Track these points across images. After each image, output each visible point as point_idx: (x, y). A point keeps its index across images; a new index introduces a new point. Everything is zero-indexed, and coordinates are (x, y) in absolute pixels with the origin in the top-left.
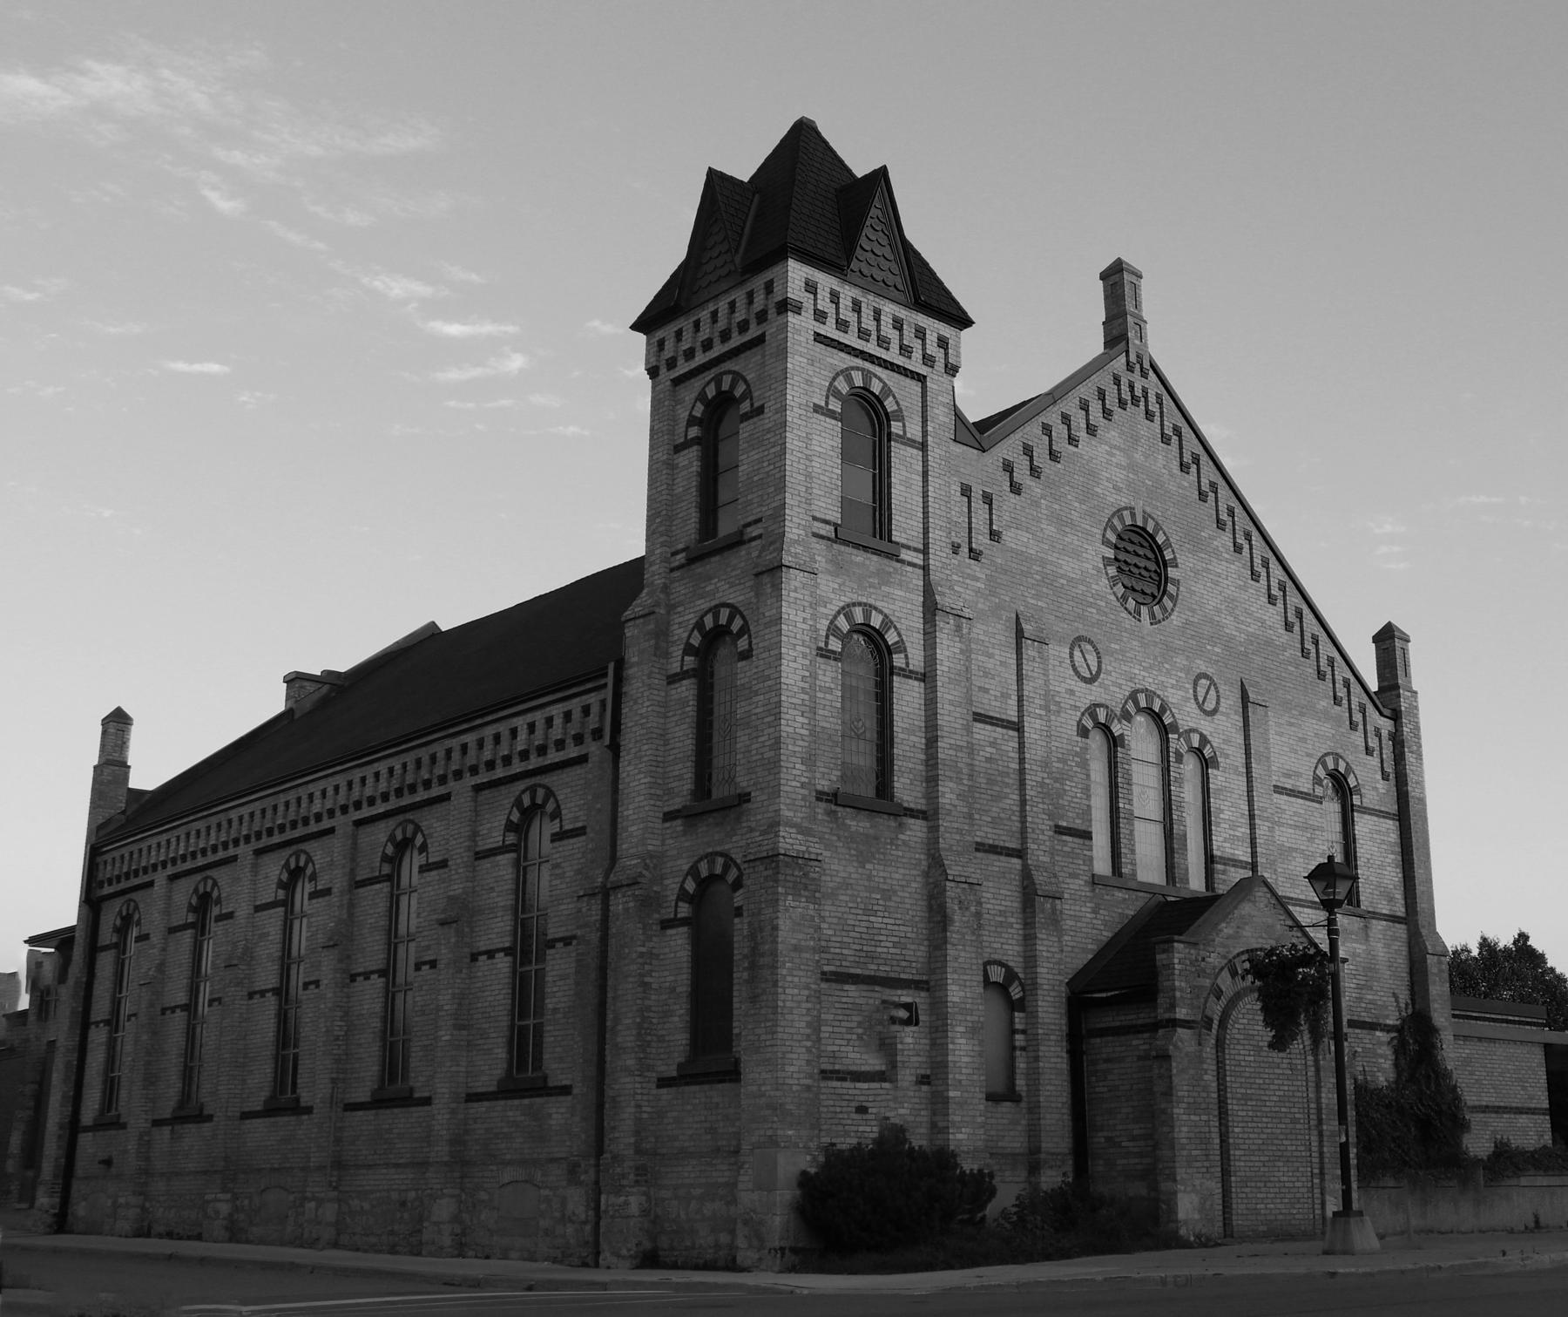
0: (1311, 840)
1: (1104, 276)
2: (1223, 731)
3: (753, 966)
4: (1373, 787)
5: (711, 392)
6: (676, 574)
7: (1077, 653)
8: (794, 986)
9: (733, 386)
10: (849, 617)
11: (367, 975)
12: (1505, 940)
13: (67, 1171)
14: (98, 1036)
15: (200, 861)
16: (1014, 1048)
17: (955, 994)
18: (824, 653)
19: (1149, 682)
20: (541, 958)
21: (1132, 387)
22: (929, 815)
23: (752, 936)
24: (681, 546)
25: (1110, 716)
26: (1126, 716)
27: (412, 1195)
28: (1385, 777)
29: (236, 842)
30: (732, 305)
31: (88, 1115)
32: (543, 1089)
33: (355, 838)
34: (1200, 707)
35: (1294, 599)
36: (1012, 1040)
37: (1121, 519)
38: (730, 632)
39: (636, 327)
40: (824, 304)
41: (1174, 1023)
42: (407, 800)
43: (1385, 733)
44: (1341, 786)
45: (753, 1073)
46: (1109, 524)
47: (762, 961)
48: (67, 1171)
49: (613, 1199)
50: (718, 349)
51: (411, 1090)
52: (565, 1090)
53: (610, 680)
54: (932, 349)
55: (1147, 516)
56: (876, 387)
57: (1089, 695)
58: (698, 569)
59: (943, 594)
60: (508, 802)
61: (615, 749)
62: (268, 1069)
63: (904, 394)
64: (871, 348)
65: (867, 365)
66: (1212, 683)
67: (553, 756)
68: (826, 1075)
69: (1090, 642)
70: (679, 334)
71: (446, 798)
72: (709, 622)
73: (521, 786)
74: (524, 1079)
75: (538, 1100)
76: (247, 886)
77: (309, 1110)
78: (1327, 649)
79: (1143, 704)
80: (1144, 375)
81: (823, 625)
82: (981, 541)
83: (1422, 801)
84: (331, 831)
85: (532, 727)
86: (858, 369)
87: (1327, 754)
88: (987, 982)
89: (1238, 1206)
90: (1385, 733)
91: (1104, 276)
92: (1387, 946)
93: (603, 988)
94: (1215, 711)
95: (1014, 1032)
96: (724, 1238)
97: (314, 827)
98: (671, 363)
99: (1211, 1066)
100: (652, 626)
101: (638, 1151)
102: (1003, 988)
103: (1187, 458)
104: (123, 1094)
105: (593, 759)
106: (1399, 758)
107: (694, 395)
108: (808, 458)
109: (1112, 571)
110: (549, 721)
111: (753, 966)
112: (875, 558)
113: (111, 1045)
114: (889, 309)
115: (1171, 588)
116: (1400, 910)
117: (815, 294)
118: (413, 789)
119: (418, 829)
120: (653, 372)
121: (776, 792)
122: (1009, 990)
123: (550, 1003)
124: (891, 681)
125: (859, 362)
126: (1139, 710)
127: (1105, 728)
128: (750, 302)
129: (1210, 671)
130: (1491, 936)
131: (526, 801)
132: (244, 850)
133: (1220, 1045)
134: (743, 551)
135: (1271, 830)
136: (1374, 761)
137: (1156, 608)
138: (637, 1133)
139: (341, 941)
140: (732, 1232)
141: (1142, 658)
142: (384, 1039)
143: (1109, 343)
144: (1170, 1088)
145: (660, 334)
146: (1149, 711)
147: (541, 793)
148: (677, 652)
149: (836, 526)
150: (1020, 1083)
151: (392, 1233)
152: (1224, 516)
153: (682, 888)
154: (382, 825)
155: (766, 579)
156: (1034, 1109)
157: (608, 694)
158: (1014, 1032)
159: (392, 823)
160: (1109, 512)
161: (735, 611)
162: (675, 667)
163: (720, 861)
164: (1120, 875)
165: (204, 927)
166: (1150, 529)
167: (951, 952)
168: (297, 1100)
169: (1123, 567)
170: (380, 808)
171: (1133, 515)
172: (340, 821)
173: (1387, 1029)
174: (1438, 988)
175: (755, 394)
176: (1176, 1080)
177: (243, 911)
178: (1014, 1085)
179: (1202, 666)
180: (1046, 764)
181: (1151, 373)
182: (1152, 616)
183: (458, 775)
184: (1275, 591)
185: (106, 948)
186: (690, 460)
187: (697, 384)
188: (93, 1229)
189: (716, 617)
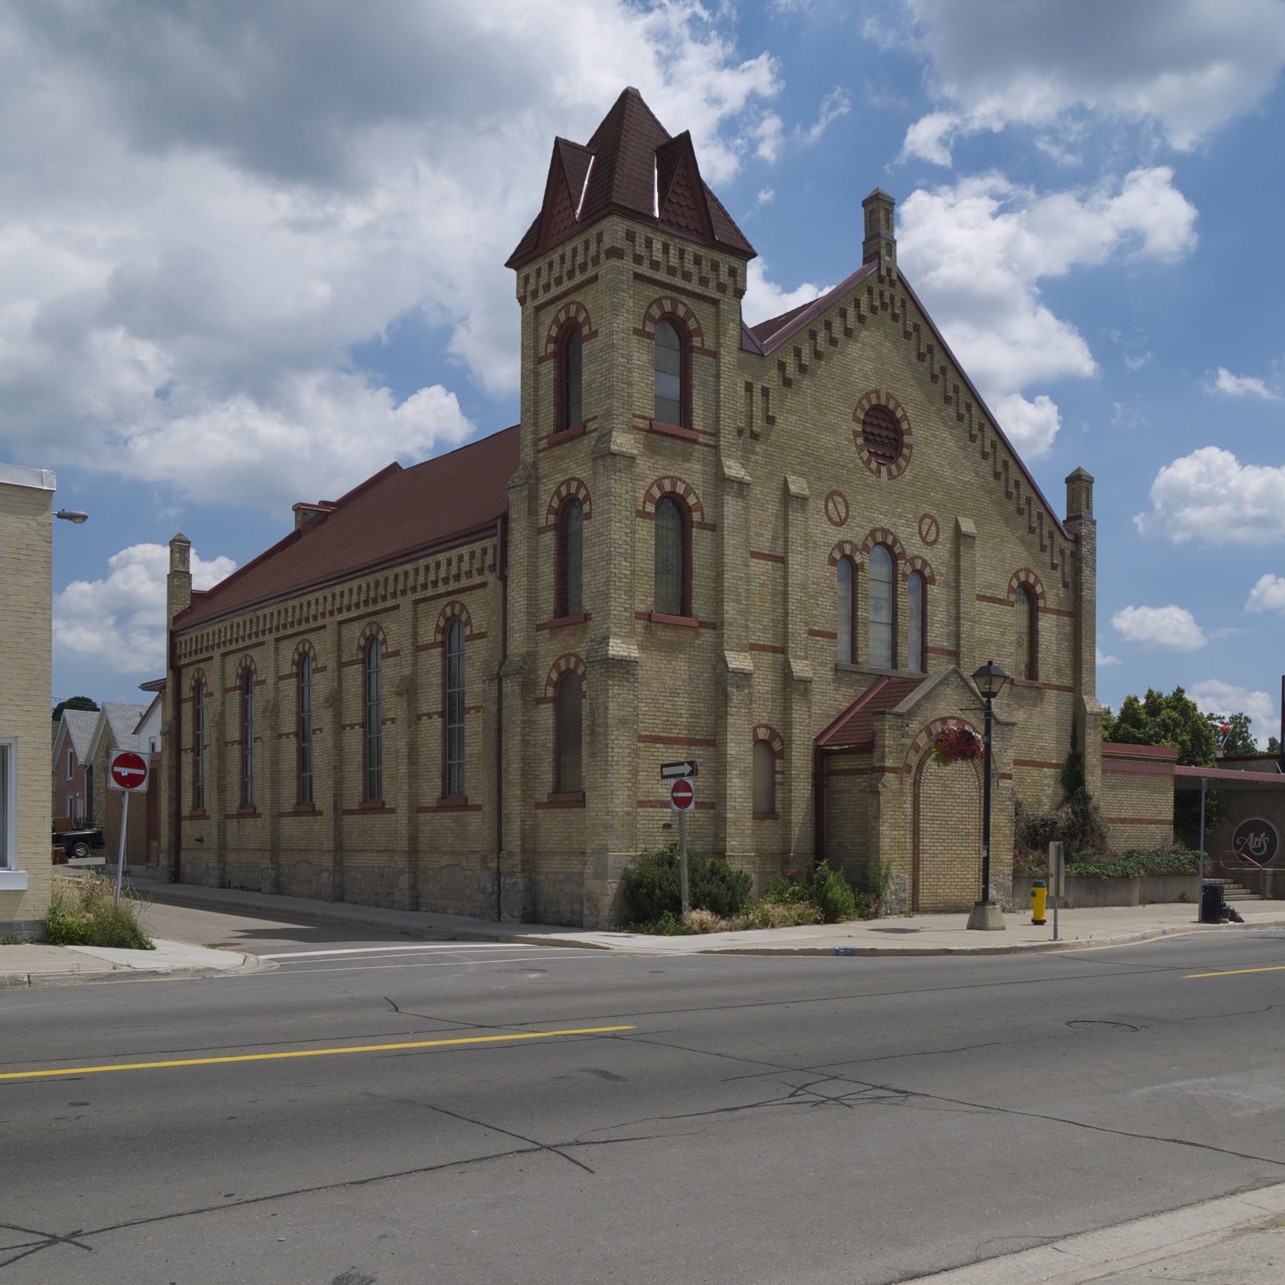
0: (1003, 634)
1: (865, 203)
2: (938, 557)
3: (593, 733)
4: (1052, 594)
5: (562, 317)
6: (541, 455)
7: (831, 504)
8: (619, 745)
9: (577, 313)
10: (660, 487)
11: (352, 726)
12: (1168, 692)
13: (177, 845)
14: (187, 759)
15: (241, 645)
16: (775, 784)
17: (732, 749)
18: (643, 514)
19: (885, 523)
20: (462, 720)
21: (881, 295)
22: (716, 625)
23: (592, 712)
24: (544, 434)
25: (855, 548)
26: (866, 548)
27: (387, 870)
28: (1065, 585)
29: (264, 633)
30: (575, 251)
31: (186, 808)
32: (465, 806)
33: (339, 632)
34: (923, 539)
35: (1002, 454)
36: (774, 778)
37: (869, 400)
39: (508, 265)
40: (641, 249)
41: (883, 770)
42: (372, 608)
43: (1067, 552)
44: (1028, 593)
45: (593, 803)
46: (860, 405)
47: (600, 730)
48: (177, 845)
49: (508, 880)
50: (567, 285)
51: (384, 803)
52: (478, 808)
53: (499, 529)
54: (724, 278)
55: (889, 396)
56: (681, 311)
57: (836, 535)
58: (557, 451)
59: (729, 467)
60: (437, 613)
61: (503, 578)
62: (294, 785)
63: (703, 313)
64: (678, 281)
65: (675, 295)
66: (934, 521)
67: (465, 582)
68: (642, 804)
69: (840, 495)
70: (539, 272)
71: (397, 607)
73: (445, 601)
74: (452, 799)
75: (464, 813)
76: (273, 663)
77: (321, 813)
78: (1025, 491)
79: (879, 539)
80: (892, 284)
81: (641, 494)
82: (759, 424)
83: (1093, 603)
84: (324, 627)
85: (449, 562)
86: (667, 298)
87: (1020, 570)
88: (757, 741)
89: (924, 885)
90: (1067, 552)
91: (865, 203)
92: (1057, 708)
93: (499, 742)
94: (935, 542)
95: (775, 772)
96: (577, 907)
97: (312, 624)
98: (535, 294)
99: (909, 799)
100: (526, 493)
101: (523, 850)
102: (766, 743)
103: (923, 349)
104: (206, 797)
105: (491, 585)
106: (1077, 571)
107: (550, 320)
108: (630, 371)
109: (860, 441)
110: (461, 558)
111: (593, 733)
112: (680, 442)
113: (196, 765)
114: (691, 249)
115: (906, 451)
116: (1067, 681)
117: (633, 241)
118: (375, 600)
119: (380, 628)
120: (522, 300)
121: (607, 615)
122: (772, 747)
123: (468, 750)
124: (691, 532)
125: (669, 293)
126: (877, 544)
127: (849, 558)
128: (587, 249)
129: (933, 512)
130: (1156, 690)
131: (449, 613)
132: (269, 638)
133: (917, 784)
134: (585, 440)
135: (972, 628)
136: (1058, 574)
137: (893, 467)
138: (522, 839)
139: (335, 701)
140: (582, 903)
141: (883, 506)
142: (365, 768)
143: (866, 260)
144: (878, 812)
145: (526, 271)
146: (884, 544)
147: (457, 607)
148: (543, 511)
149: (651, 420)
150: (778, 806)
151: (376, 893)
152: (950, 393)
153: (549, 677)
154: (356, 624)
155: (600, 462)
156: (787, 823)
157: (496, 540)
158: (775, 772)
159: (363, 623)
160: (859, 395)
161: (581, 484)
162: (542, 523)
163: (573, 659)
164: (857, 663)
165: (247, 689)
166: (891, 406)
167: (730, 720)
168: (314, 806)
169: (869, 437)
170: (354, 613)
171: (878, 397)
172: (328, 620)
173: (1051, 766)
174: (1093, 740)
175: (593, 321)
176: (882, 809)
177: (271, 681)
178: (774, 804)
179: (927, 509)
180: (804, 586)
181: (898, 283)
182: (890, 473)
183: (404, 592)
184: (988, 449)
185: (187, 700)
186: (548, 369)
187: (553, 309)
188: (196, 882)
189: (569, 487)
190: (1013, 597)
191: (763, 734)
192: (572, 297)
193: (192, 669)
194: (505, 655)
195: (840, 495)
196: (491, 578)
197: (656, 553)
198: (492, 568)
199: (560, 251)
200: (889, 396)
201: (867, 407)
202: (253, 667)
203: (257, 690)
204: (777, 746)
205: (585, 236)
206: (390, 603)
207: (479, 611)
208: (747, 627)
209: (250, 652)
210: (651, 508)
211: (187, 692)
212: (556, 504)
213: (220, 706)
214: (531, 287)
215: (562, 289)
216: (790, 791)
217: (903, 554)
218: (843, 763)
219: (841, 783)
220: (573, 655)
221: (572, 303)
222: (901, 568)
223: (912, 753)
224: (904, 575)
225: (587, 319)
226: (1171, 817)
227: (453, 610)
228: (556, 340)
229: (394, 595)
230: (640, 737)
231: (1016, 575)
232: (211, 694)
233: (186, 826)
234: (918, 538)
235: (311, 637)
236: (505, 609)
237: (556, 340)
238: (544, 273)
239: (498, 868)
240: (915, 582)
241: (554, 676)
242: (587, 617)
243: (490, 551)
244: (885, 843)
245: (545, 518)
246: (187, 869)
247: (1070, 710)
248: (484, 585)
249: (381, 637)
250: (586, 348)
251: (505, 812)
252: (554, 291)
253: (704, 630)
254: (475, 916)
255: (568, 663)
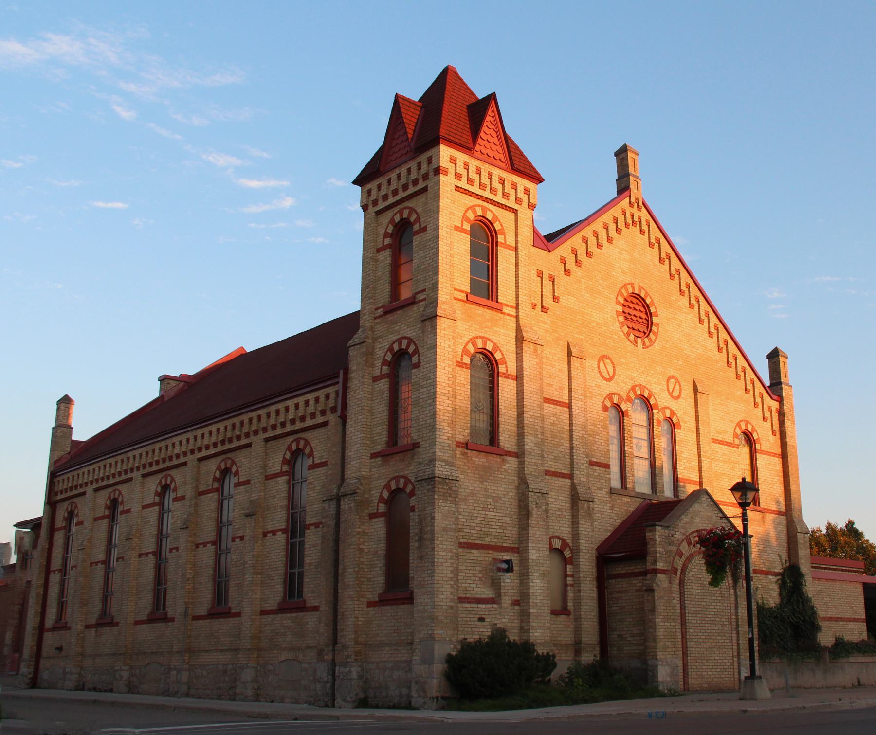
0: (732, 469)
2: (683, 409)
3: (421, 539)
4: (767, 440)
5: (397, 219)
7: (602, 365)
8: (444, 549)
9: (410, 215)
10: (474, 344)
11: (205, 544)
12: (841, 524)
14: (55, 578)
15: (112, 481)
16: (566, 585)
17: (533, 555)
18: (460, 364)
19: (642, 380)
20: (302, 535)
21: (632, 216)
23: (420, 522)
24: (380, 305)
26: (629, 399)
27: (230, 667)
29: (132, 470)
30: (409, 170)
31: (49, 623)
34: (671, 394)
36: (566, 581)
37: (627, 290)
38: (408, 353)
40: (461, 170)
41: (656, 571)
42: (228, 446)
43: (774, 410)
44: (749, 439)
45: (421, 599)
46: (620, 293)
49: (342, 669)
50: (402, 195)
52: (316, 609)
53: (341, 379)
55: (640, 288)
56: (489, 216)
57: (608, 388)
58: (390, 317)
59: (527, 332)
60: (283, 448)
61: (343, 419)
64: (487, 194)
65: (485, 204)
67: (309, 422)
68: (462, 600)
69: (609, 358)
71: (249, 445)
72: (396, 347)
73: (291, 438)
74: (293, 600)
75: (301, 614)
76: (139, 494)
77: (172, 620)
79: (639, 393)
81: (460, 349)
86: (479, 206)
87: (741, 421)
88: (552, 549)
90: (774, 410)
93: (337, 552)
94: (679, 397)
95: (566, 576)
96: (404, 691)
97: (175, 462)
98: (375, 203)
99: (677, 595)
102: (560, 552)
103: (663, 255)
105: (332, 424)
106: (782, 423)
107: (388, 220)
108: (451, 256)
109: (622, 319)
111: (421, 539)
113: (62, 583)
114: (497, 173)
119: (233, 462)
120: (365, 208)
122: (563, 554)
123: (307, 560)
125: (480, 202)
127: (617, 407)
129: (676, 375)
130: (833, 522)
132: (136, 475)
133: (682, 583)
134: (415, 308)
135: (710, 463)
137: (646, 340)
140: (409, 688)
142: (214, 580)
144: (654, 607)
145: (369, 186)
147: (302, 443)
148: (378, 364)
150: (570, 604)
151: (219, 688)
153: (381, 496)
156: (578, 619)
157: (339, 387)
158: (566, 576)
159: (219, 459)
160: (619, 286)
161: (411, 341)
162: (377, 372)
163: (402, 480)
164: (626, 488)
168: (166, 614)
169: (627, 316)
170: (212, 451)
171: (633, 288)
175: (422, 220)
176: (657, 602)
179: (671, 372)
181: (643, 208)
182: (644, 343)
183: (256, 432)
187: (389, 214)
188: (52, 686)
189: (400, 344)
190: (737, 441)
191: (557, 544)
192: (408, 204)
193: (66, 504)
194: (343, 479)
195: (609, 358)
196: (332, 418)
197: (471, 395)
198: (334, 410)
199: (397, 171)
200: (640, 288)
201: (625, 294)
202: (120, 499)
203: (121, 518)
204: (567, 554)
205: (418, 160)
206: (244, 441)
207: (320, 444)
208: (543, 456)
209: (119, 487)
210: (467, 360)
211: (60, 522)
212: (389, 357)
213: (89, 535)
214: (373, 197)
215: (398, 198)
216: (579, 591)
217: (656, 405)
218: (621, 569)
219: (617, 585)
220: (403, 477)
221: (405, 208)
222: (655, 416)
223: (677, 557)
224: (658, 420)
225: (418, 220)
226: (864, 617)
227: (298, 445)
228: (391, 235)
229: (247, 435)
230: (460, 543)
231: (738, 425)
232: (80, 523)
233: (47, 636)
234: (666, 393)
235: (173, 472)
236: (344, 442)
237: (391, 235)
238: (384, 187)
239: (333, 660)
240: (666, 426)
241: (386, 494)
242: (416, 445)
243: (332, 396)
244: (660, 632)
245: (378, 369)
246: (45, 675)
247: (785, 530)
248: (325, 424)
249: (234, 469)
250: (416, 240)
251: (340, 610)
252: (391, 200)
253: (509, 458)
254: (310, 703)
255: (397, 483)
